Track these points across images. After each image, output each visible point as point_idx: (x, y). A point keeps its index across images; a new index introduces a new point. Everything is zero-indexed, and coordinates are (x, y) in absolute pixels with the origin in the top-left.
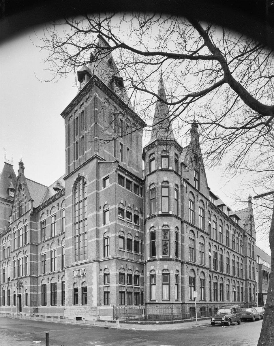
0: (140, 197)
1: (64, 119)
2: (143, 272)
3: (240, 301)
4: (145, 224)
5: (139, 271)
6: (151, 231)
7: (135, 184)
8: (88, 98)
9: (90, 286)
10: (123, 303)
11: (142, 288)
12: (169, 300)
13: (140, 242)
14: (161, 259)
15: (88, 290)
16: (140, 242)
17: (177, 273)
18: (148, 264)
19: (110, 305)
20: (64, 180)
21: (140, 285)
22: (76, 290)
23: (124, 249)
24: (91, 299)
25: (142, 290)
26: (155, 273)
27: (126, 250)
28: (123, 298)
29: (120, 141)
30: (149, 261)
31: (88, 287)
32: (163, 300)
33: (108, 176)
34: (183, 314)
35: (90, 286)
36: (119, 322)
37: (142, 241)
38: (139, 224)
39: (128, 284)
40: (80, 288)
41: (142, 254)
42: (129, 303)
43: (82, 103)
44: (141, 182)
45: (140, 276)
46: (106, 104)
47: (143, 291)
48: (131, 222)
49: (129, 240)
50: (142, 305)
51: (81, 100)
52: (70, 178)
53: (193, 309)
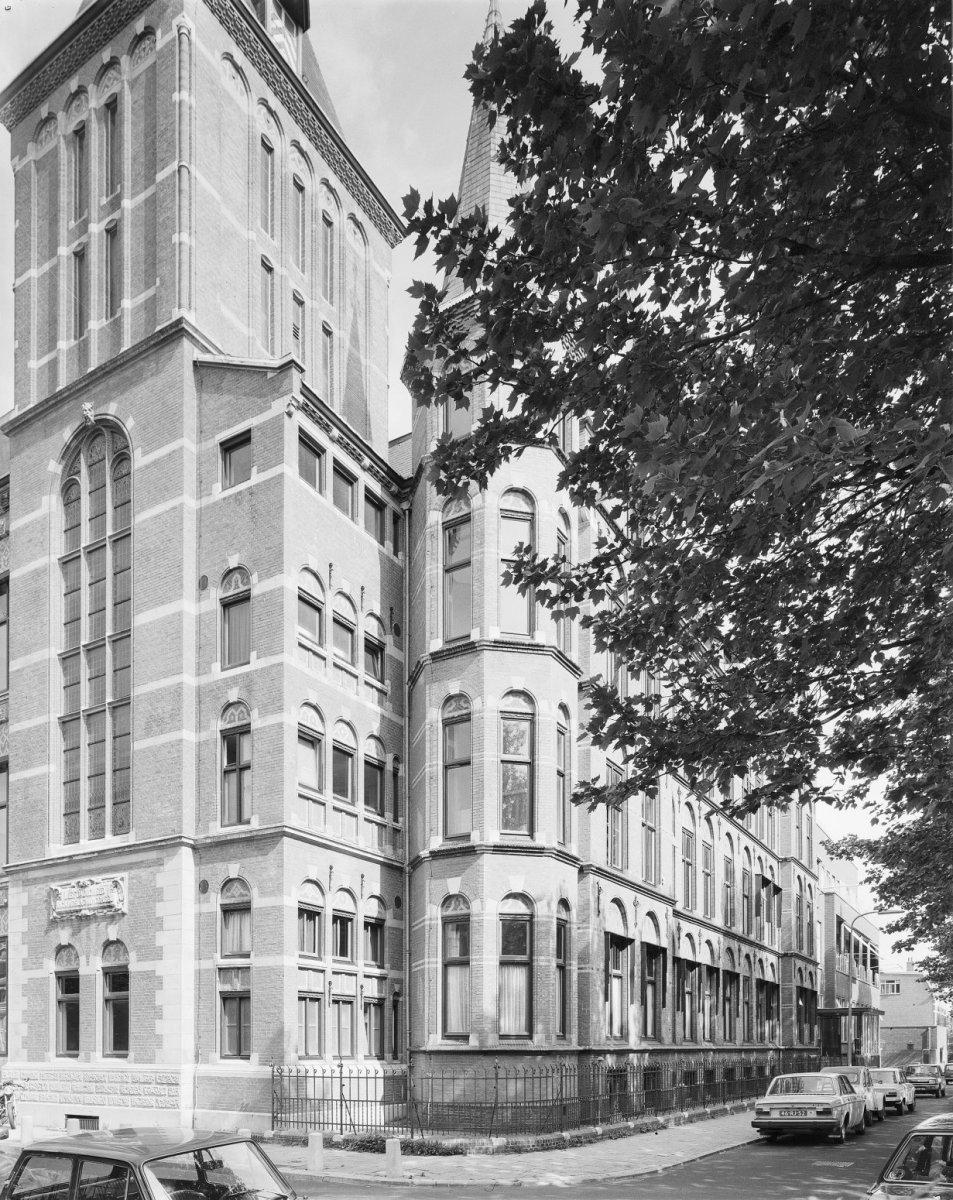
0: (392, 557)
1: (10, 129)
2: (398, 902)
3: (574, 1037)
4: (413, 680)
5: (386, 898)
6: (446, 716)
7: (368, 492)
8: (140, 38)
9: (146, 966)
10: (313, 1052)
11: (400, 981)
12: (530, 1037)
13: (389, 767)
14: (499, 849)
15: (133, 983)
16: (389, 767)
17: (564, 916)
18: (426, 868)
19: (255, 1057)
20: (7, 434)
21: (387, 965)
22: (70, 982)
23: (320, 791)
24: (152, 1028)
25: (397, 988)
26: (465, 911)
27: (328, 795)
28: (314, 1024)
29: (293, 285)
30: (435, 855)
31: (135, 967)
32: (502, 1037)
33: (249, 431)
34: (584, 1102)
35: (146, 966)
36: (320, 1143)
37: (397, 759)
38: (387, 682)
39: (306, 953)
40: (92, 968)
41: (396, 820)
42: (240, 1051)
43: (44, 114)
44: (394, 488)
45: (390, 922)
46: (230, 83)
47: (397, 994)
48: (349, 668)
49: (342, 753)
50: (395, 1057)
51: (108, 38)
52: (39, 424)
53: (618, 1076)
